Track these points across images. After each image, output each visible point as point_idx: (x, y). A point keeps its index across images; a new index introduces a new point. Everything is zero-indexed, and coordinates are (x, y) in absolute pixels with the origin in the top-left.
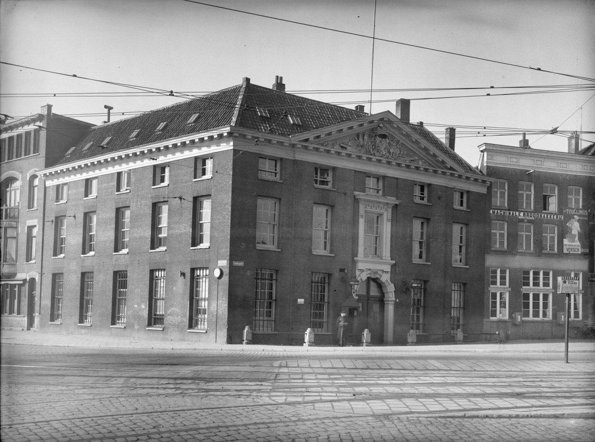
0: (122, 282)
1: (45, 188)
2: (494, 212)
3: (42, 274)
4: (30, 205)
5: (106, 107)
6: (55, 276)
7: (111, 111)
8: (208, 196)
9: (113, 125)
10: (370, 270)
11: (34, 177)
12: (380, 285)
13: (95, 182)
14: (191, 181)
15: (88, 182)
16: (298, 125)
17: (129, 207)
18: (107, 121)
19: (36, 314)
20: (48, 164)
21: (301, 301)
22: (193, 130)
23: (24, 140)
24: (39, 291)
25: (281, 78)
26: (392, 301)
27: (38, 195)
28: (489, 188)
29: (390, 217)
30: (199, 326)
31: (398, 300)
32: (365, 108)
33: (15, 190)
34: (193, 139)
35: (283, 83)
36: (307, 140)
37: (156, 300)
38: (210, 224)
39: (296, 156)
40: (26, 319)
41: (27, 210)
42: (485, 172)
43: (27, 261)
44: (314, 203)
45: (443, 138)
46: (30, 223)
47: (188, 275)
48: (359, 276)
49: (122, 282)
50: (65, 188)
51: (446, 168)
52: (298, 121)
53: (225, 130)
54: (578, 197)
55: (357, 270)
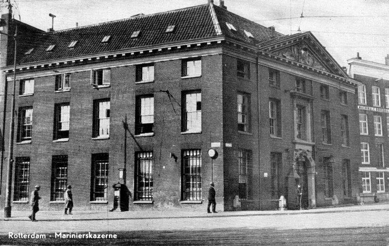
1: (7, 83)
5: (50, 15)
7: (54, 18)
8: (67, 104)
21: (266, 175)
30: (191, 198)
47: (179, 155)
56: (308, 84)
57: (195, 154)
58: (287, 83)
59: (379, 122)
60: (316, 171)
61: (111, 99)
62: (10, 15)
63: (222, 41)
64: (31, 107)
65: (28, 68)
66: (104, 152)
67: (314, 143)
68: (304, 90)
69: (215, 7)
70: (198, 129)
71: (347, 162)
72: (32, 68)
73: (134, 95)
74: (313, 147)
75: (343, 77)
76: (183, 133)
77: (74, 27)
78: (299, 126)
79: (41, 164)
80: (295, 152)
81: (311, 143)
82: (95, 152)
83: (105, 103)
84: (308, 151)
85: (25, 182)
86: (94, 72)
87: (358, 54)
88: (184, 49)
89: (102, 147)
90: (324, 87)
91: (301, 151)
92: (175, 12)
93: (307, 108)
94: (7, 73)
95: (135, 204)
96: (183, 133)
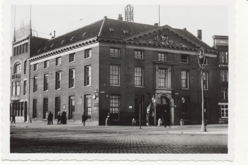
1: (30, 66)
2: (221, 66)
3: (29, 99)
4: (25, 73)
9: (57, 39)
10: (162, 93)
12: (168, 100)
13: (48, 62)
14: (83, 60)
15: (45, 62)
16: (127, 34)
18: (54, 36)
19: (28, 116)
20: (31, 56)
22: (84, 39)
23: (22, 47)
25: (121, 15)
26: (173, 106)
27: (28, 68)
28: (218, 55)
29: (170, 70)
31: (175, 106)
32: (187, 29)
33: (19, 67)
35: (122, 17)
36: (131, 40)
37: (87, 108)
40: (24, 118)
42: (216, 48)
43: (24, 95)
44: (135, 66)
45: (196, 35)
46: (25, 80)
48: (157, 96)
50: (37, 65)
51: (196, 47)
52: (127, 32)
53: (95, 38)
54: (138, 120)
55: (156, 94)
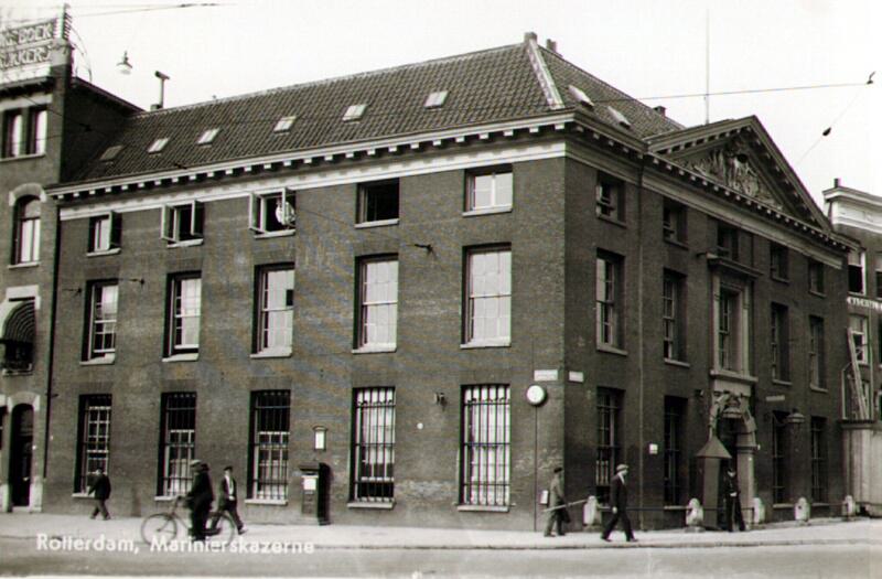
0: (277, 415)
1: (59, 223)
3: (50, 396)
5: (158, 74)
6: (87, 400)
7: (166, 82)
8: (195, 274)
11: (25, 200)
17: (397, 254)
24: (44, 431)
34: (525, 126)
38: (509, 299)
39: (644, 180)
41: (10, 266)
49: (277, 415)
56: (743, 241)
57: (493, 396)
58: (700, 236)
59: (861, 330)
60: (757, 443)
61: (297, 263)
62: (69, 68)
63: (567, 124)
64: (113, 282)
65: (108, 190)
66: (280, 387)
67: (755, 379)
68: (736, 257)
69: (540, 48)
70: (503, 337)
71: (818, 422)
72: (117, 190)
73: (353, 256)
74: (753, 386)
75: (820, 227)
76: (255, 356)
77: (211, 99)
78: (723, 336)
79: (138, 407)
80: (714, 399)
81: (747, 377)
82: (259, 387)
83: (282, 274)
84: (742, 396)
85: (100, 451)
86: (258, 201)
87: (837, 181)
88: (471, 144)
89: (272, 380)
90: (777, 250)
91: (727, 396)
92: (445, 62)
93: (741, 295)
94: (61, 200)
95: (351, 508)
96: (255, 356)
